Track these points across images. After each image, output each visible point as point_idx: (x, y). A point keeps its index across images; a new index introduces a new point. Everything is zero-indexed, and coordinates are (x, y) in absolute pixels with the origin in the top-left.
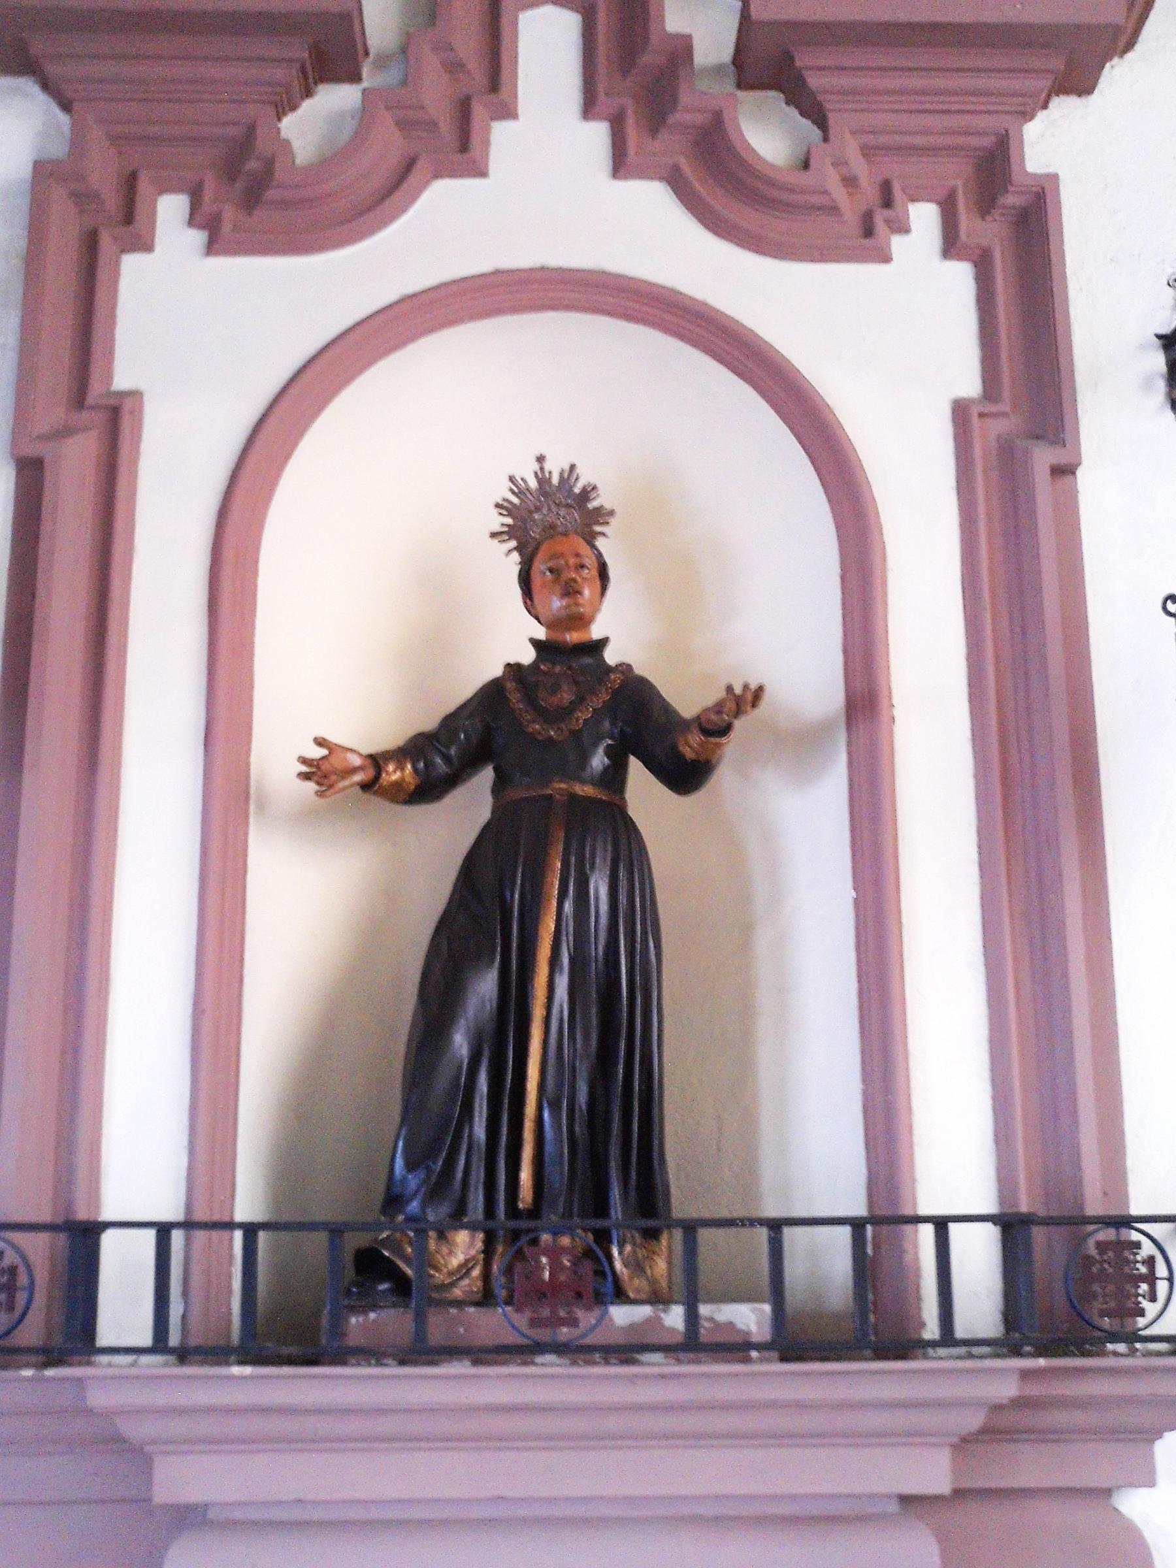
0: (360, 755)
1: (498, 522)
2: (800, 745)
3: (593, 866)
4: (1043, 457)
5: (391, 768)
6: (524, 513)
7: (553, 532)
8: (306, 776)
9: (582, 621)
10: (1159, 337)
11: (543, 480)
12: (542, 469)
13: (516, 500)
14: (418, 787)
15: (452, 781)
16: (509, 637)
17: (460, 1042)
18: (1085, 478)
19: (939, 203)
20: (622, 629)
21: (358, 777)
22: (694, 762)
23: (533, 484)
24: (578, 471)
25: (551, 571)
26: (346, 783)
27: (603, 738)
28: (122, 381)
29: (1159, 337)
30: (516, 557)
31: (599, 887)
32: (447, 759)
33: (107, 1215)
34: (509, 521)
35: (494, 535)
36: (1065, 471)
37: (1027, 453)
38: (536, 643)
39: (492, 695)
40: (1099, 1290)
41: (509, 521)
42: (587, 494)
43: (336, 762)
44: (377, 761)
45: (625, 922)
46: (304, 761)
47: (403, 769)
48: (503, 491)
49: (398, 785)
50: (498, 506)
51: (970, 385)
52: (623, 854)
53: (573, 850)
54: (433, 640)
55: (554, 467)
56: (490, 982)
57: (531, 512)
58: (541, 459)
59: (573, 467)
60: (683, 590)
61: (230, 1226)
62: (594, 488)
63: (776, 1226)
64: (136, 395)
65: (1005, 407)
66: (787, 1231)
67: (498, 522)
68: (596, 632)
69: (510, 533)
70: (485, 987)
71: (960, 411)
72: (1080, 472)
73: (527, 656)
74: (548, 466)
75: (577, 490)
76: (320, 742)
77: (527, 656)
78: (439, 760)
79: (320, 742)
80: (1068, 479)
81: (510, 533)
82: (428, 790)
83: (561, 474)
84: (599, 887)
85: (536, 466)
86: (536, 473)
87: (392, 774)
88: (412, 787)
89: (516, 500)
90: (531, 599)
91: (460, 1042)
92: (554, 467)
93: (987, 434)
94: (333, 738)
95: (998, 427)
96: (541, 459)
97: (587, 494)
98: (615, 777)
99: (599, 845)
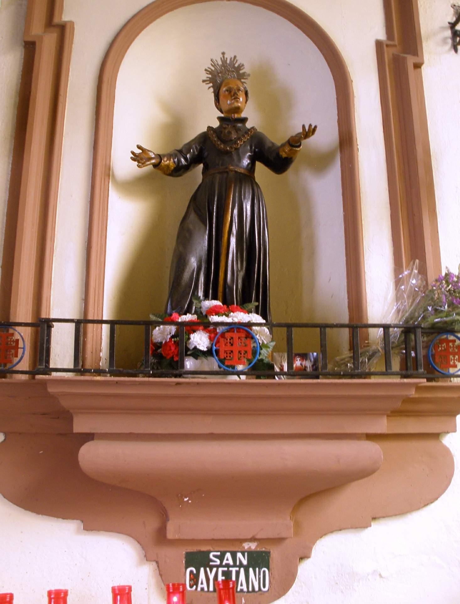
0: (154, 153)
1: (205, 76)
2: (321, 163)
3: (245, 198)
4: (411, 60)
5: (165, 159)
6: (216, 74)
7: (225, 81)
8: (133, 159)
9: (238, 110)
10: (449, 23)
11: (224, 61)
12: (224, 57)
13: (213, 69)
14: (175, 168)
15: (187, 168)
16: (208, 118)
17: (193, 262)
18: (425, 69)
19: (279, 148)
20: (252, 116)
21: (153, 161)
22: (286, 158)
23: (220, 63)
24: (237, 58)
25: (227, 91)
26: (148, 163)
27: (247, 153)
28: (66, 18)
29: (449, 23)
30: (212, 90)
31: (247, 206)
32: (186, 159)
33: (53, 316)
34: (210, 76)
35: (204, 81)
36: (418, 66)
37: (404, 59)
38: (220, 119)
39: (204, 138)
40: (453, 358)
41: (210, 76)
42: (240, 67)
43: (144, 156)
44: (160, 157)
45: (257, 218)
46: (133, 153)
47: (170, 160)
48: (208, 65)
49: (168, 166)
50: (206, 70)
51: (382, 35)
52: (256, 194)
53: (237, 190)
54: (175, 125)
55: (228, 56)
56: (198, 251)
57: (218, 73)
58: (223, 54)
59: (235, 57)
60: (278, 102)
61: (102, 322)
62: (243, 65)
63: (323, 327)
64: (72, 23)
65: (396, 42)
66: (328, 330)
67: (205, 76)
68: (243, 115)
69: (211, 80)
70: (201, 244)
71: (379, 44)
72: (423, 67)
73: (216, 124)
74: (225, 56)
75: (236, 65)
76: (139, 147)
77: (216, 124)
78: (183, 160)
79: (139, 147)
80: (419, 70)
81: (211, 80)
82: (178, 171)
83: (231, 59)
84: (247, 206)
85: (222, 56)
86: (221, 58)
87: (165, 162)
88: (173, 168)
89: (213, 69)
90: (219, 103)
91: (193, 262)
92: (228, 56)
93: (388, 54)
94: (144, 146)
95: (393, 51)
96: (223, 54)
97: (240, 67)
98: (251, 168)
99: (247, 190)
